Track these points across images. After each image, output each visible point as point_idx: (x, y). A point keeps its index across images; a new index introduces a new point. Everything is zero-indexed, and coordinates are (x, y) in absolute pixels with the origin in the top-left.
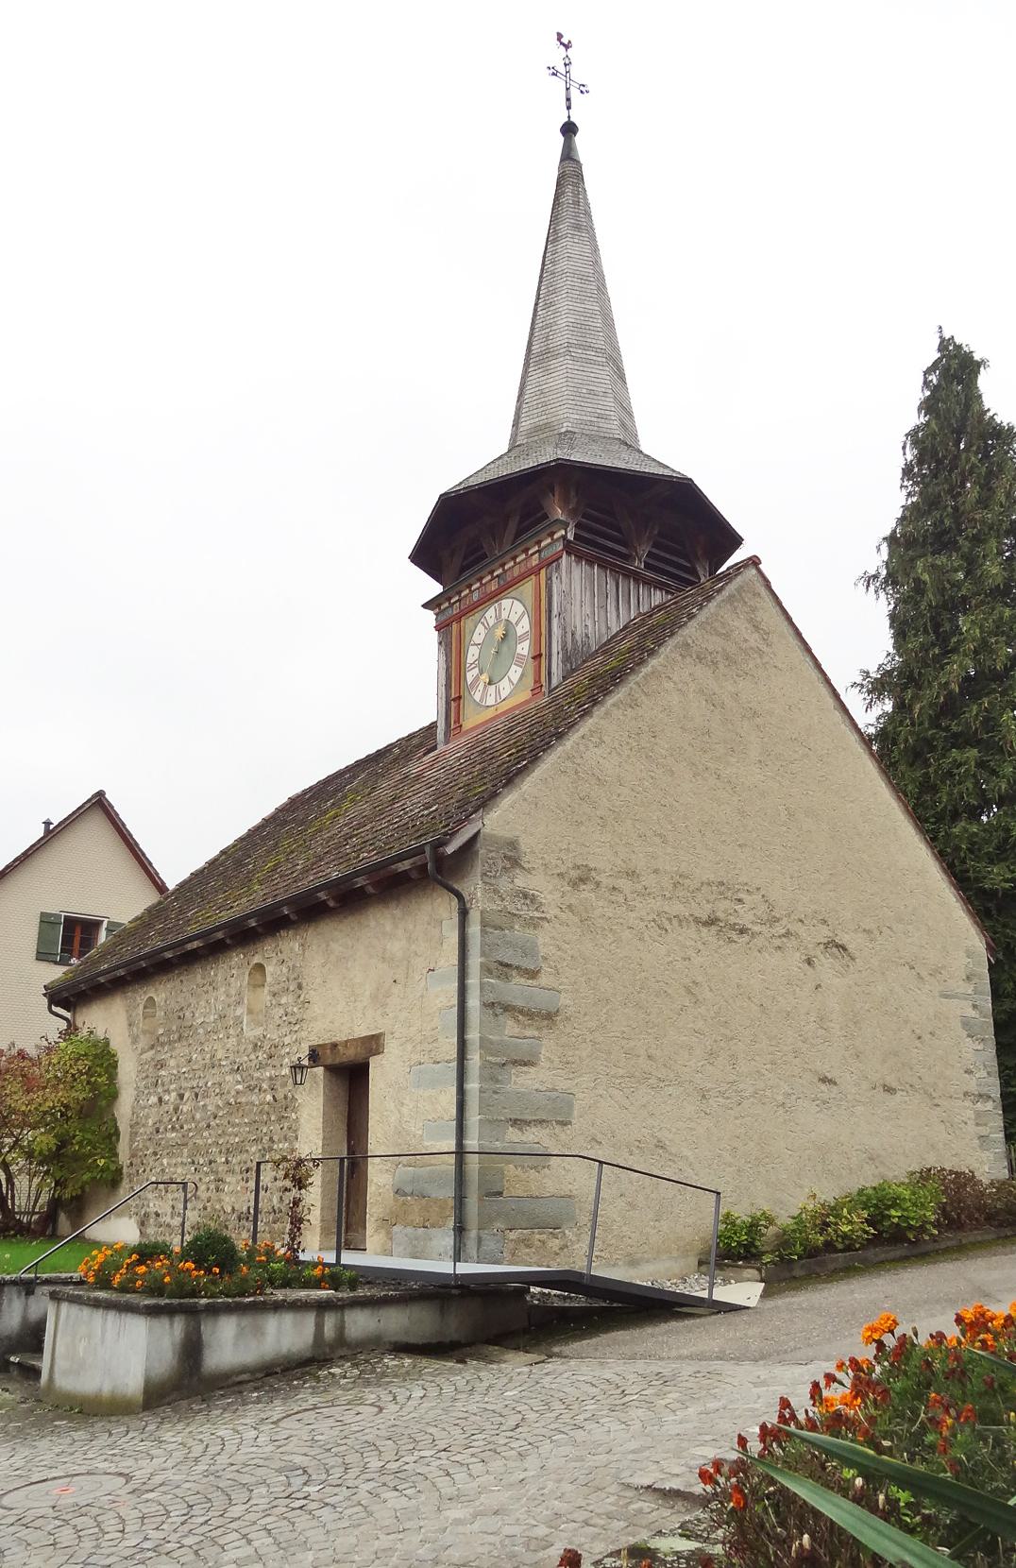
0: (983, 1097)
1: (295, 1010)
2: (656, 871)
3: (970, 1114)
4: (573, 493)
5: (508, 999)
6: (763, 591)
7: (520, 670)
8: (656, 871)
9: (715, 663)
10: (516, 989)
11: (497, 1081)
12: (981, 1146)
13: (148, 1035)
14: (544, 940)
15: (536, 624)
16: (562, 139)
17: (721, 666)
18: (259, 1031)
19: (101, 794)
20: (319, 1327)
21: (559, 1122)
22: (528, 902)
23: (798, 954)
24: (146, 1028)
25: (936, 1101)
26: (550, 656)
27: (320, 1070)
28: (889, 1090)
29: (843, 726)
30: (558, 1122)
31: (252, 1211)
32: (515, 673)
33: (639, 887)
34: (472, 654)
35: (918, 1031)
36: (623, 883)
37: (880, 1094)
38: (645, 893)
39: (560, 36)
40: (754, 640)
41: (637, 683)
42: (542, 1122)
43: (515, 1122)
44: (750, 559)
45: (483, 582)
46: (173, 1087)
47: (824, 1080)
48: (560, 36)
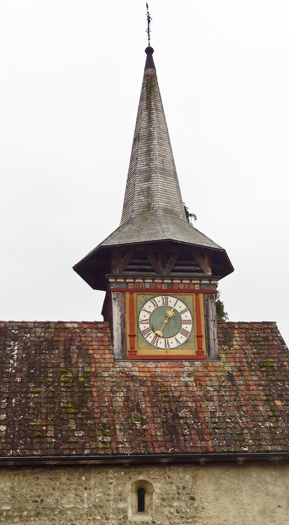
16: (146, 55)
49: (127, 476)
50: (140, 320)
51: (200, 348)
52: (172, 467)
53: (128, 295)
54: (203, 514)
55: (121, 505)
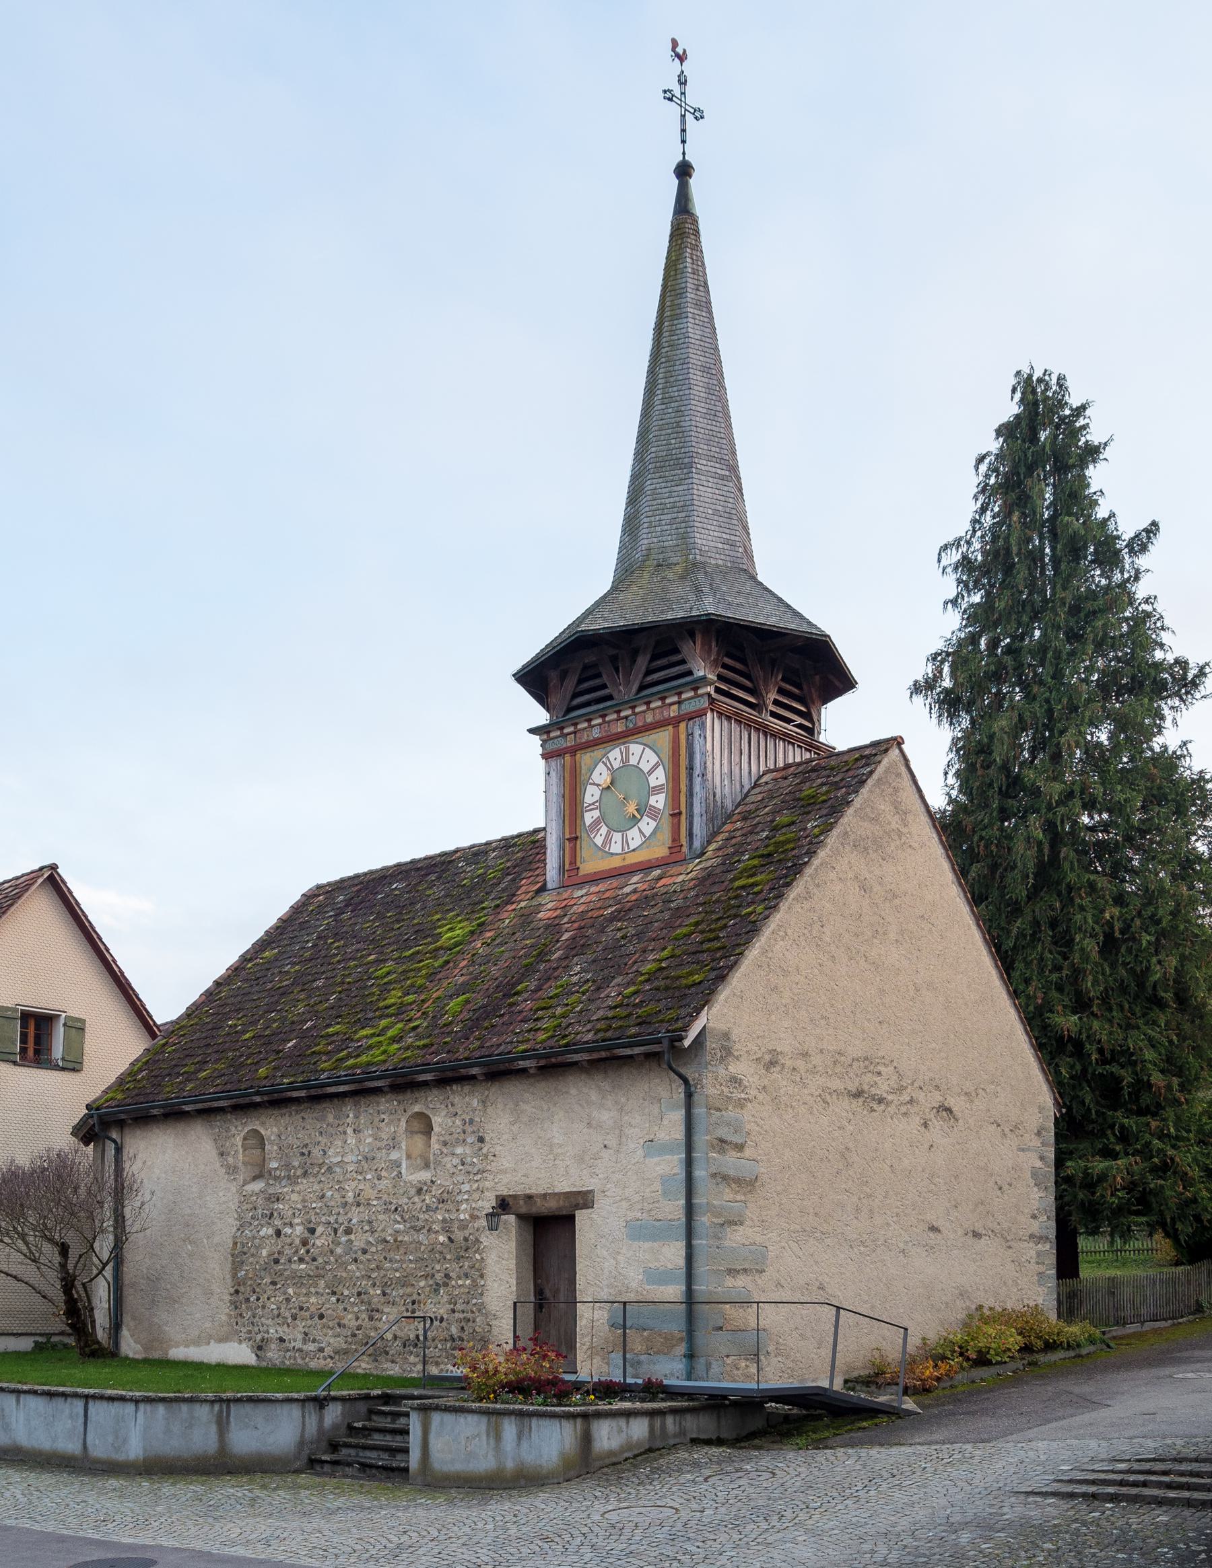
0: (1041, 1239)
1: (475, 1160)
3: (1033, 1253)
4: (714, 644)
5: (724, 1170)
6: (903, 770)
7: (653, 824)
8: (821, 1051)
9: (866, 849)
10: (730, 1162)
11: (719, 1239)
12: (1039, 1281)
13: (249, 1167)
14: (747, 1115)
15: (674, 778)
16: (677, 182)
18: (425, 1175)
19: (54, 867)
20: (652, 1428)
21: (757, 1271)
23: (918, 1118)
24: (247, 1159)
25: (1009, 1243)
27: (511, 1218)
28: (977, 1235)
30: (757, 1271)
31: (421, 1338)
34: (591, 795)
36: (801, 1064)
37: (970, 1240)
38: (813, 1071)
39: (675, 43)
40: (895, 821)
42: (745, 1270)
44: (894, 739)
46: (297, 1221)
47: (933, 1229)
48: (675, 43)
50: (585, 805)
51: (676, 838)
52: (454, 1087)
55: (394, 1155)
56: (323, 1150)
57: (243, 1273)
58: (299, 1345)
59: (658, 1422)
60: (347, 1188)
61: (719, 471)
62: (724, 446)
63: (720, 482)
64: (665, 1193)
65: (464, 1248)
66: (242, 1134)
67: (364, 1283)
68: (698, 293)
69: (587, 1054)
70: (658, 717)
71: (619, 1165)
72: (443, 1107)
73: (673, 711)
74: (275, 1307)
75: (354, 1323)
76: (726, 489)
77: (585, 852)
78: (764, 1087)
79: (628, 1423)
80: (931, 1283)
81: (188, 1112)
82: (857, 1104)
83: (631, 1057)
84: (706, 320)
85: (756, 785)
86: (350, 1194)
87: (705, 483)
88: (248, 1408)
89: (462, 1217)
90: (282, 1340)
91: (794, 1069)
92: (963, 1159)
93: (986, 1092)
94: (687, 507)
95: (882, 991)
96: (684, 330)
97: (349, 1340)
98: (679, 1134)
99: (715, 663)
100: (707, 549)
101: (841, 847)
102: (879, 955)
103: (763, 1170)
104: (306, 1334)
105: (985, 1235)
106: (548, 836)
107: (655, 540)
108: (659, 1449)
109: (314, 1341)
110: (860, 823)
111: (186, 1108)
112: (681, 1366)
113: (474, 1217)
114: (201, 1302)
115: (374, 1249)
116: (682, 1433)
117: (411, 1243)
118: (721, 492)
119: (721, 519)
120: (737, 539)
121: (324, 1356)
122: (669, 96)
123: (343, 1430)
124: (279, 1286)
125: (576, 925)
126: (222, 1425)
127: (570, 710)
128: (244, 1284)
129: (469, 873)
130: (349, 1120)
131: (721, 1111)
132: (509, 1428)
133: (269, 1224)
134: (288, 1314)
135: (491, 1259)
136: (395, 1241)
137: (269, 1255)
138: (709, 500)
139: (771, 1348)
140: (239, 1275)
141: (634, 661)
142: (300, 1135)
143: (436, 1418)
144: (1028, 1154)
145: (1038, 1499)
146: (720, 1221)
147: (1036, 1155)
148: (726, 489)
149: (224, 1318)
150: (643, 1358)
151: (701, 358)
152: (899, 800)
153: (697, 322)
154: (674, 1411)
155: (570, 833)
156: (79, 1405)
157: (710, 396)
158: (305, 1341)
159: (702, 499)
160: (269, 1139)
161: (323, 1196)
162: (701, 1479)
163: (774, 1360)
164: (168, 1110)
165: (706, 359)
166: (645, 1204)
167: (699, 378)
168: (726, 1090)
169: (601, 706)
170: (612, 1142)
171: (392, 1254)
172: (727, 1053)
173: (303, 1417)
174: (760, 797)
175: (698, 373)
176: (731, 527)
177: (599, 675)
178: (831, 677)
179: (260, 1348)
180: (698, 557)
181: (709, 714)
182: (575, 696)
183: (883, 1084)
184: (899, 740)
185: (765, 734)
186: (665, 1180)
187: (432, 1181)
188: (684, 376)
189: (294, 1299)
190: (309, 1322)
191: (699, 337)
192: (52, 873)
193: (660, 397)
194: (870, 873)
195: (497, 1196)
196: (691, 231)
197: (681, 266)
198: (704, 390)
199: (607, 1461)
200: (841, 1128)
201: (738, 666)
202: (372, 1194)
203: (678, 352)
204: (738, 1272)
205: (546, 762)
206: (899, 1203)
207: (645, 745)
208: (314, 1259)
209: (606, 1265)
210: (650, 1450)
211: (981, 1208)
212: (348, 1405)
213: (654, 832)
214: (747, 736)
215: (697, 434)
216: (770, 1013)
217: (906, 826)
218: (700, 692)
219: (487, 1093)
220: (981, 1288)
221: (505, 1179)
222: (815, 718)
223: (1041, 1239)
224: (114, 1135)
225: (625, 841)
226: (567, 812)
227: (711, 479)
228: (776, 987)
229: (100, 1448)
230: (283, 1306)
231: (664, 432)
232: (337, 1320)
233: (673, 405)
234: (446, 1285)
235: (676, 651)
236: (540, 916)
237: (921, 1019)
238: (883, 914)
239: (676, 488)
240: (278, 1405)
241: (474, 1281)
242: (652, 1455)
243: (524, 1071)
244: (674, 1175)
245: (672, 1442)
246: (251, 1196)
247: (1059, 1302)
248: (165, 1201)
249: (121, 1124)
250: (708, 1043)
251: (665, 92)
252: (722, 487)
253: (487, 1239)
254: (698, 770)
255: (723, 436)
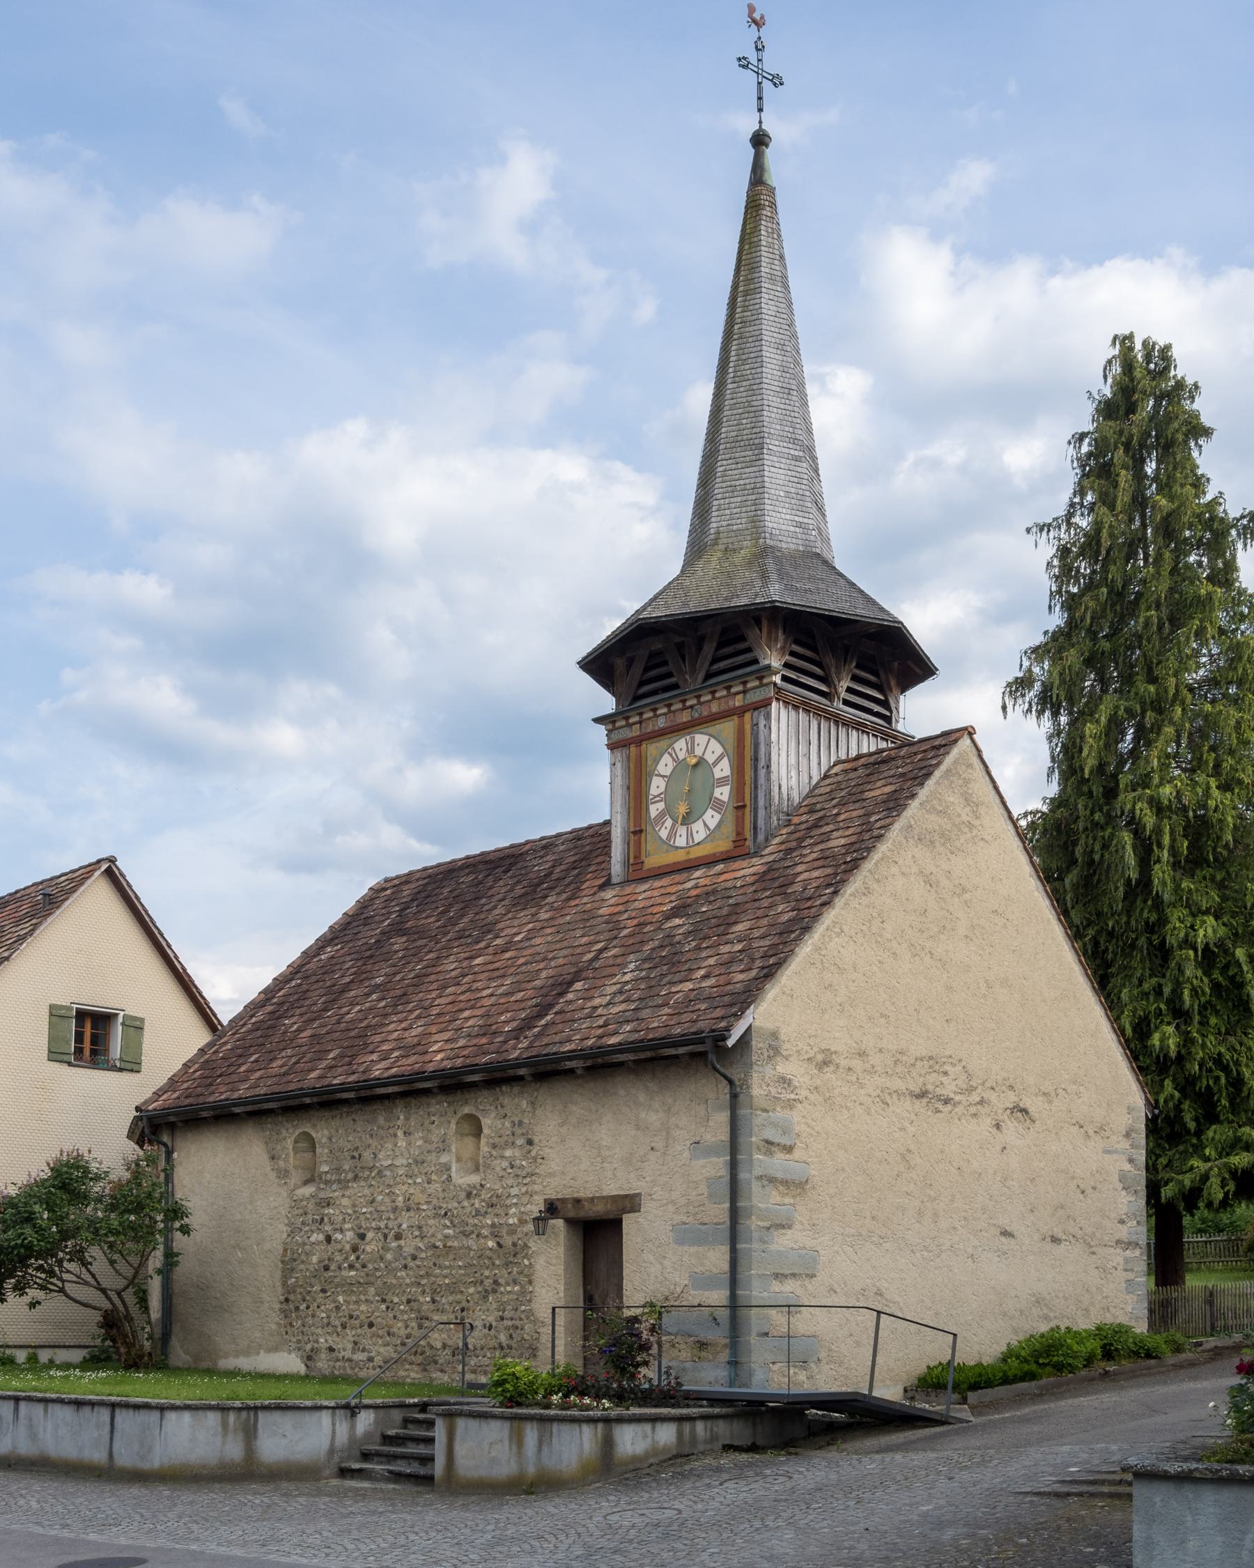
0: (1130, 1245)
1: (524, 1163)
2: (881, 1051)
3: (1121, 1260)
5: (771, 1172)
7: (718, 817)
8: (881, 1051)
9: (932, 842)
10: (777, 1163)
11: (765, 1242)
12: (1127, 1289)
14: (797, 1118)
15: (738, 769)
17: (937, 844)
18: (474, 1179)
19: (112, 860)
20: (680, 1435)
21: (807, 1275)
22: (786, 1085)
23: (989, 1120)
25: (1093, 1249)
26: (756, 809)
27: (559, 1223)
28: (1055, 1240)
29: (1036, 893)
30: (807, 1275)
32: (712, 818)
33: (868, 1066)
34: (657, 786)
35: (1082, 1186)
36: (857, 1064)
37: (1048, 1246)
38: (872, 1071)
39: (751, 9)
40: (965, 814)
41: (870, 871)
42: (794, 1275)
43: (777, 1276)
44: (965, 729)
45: (672, 709)
46: (347, 1226)
47: (1006, 1234)
48: (751, 9)
49: (452, 1109)
50: (651, 797)
52: (504, 1088)
53: (633, 748)
54: (541, 1170)
55: (444, 1159)
56: (374, 1154)
57: (293, 1280)
58: (348, 1354)
59: (687, 1427)
60: (397, 1192)
61: (792, 452)
62: (798, 426)
63: (793, 462)
64: (710, 1196)
65: (512, 1253)
66: (293, 1138)
67: (414, 1289)
68: (773, 267)
69: (633, 1054)
70: (724, 707)
71: (665, 1168)
72: (492, 1108)
73: (738, 701)
74: (324, 1315)
75: (403, 1332)
76: (799, 470)
77: (649, 845)
78: (816, 1088)
79: (653, 1429)
80: (1004, 1289)
81: (238, 1114)
82: (919, 1105)
83: (676, 1056)
84: (781, 295)
85: (826, 777)
86: (400, 1199)
87: (777, 465)
88: (277, 1416)
89: (511, 1221)
90: (331, 1349)
91: (850, 1069)
92: (1040, 1161)
93: (1067, 1093)
94: (758, 489)
95: (949, 988)
96: (757, 306)
97: (399, 1349)
98: (724, 1136)
99: (782, 651)
100: (778, 532)
101: (904, 841)
102: (947, 951)
103: (814, 1172)
104: (355, 1343)
105: (1066, 1240)
106: (613, 829)
107: (725, 523)
108: (688, 1456)
109: (363, 1350)
110: (926, 816)
111: (237, 1110)
112: (725, 1373)
113: (522, 1222)
114: (251, 1311)
115: (423, 1255)
116: (713, 1438)
117: (461, 1248)
118: (794, 474)
119: (793, 501)
120: (810, 521)
121: (373, 1366)
122: (743, 63)
123: (378, 1439)
124: (329, 1294)
125: (635, 922)
126: (250, 1434)
127: (636, 698)
128: (294, 1292)
129: (540, 867)
130: (399, 1123)
131: (767, 1111)
132: (531, 1434)
133: (320, 1229)
134: (337, 1323)
135: (540, 1264)
136: (445, 1246)
137: (320, 1262)
138: (781, 482)
139: (822, 1355)
140: (289, 1283)
141: (700, 649)
142: (350, 1138)
143: (461, 1423)
144: (1115, 1156)
145: (1035, 1499)
146: (766, 1224)
147: (1124, 1158)
148: (799, 470)
149: (274, 1327)
150: (688, 1365)
151: (775, 335)
152: (970, 791)
153: (771, 297)
154: (704, 1417)
155: (635, 826)
156: (105, 1414)
157: (784, 374)
158: (354, 1352)
159: (773, 480)
160: (320, 1142)
161: (373, 1201)
162: (717, 1483)
163: (825, 1368)
164: (218, 1112)
165: (780, 336)
166: (691, 1208)
167: (772, 356)
168: (773, 1091)
169: (667, 695)
170: (659, 1144)
171: (441, 1261)
172: (775, 1051)
173: (334, 1424)
174: (828, 789)
175: (772, 350)
176: (804, 509)
177: (665, 663)
178: (910, 663)
179: (309, 1358)
180: (768, 541)
181: (774, 704)
182: (642, 684)
183: (949, 1084)
184: (970, 729)
185: (837, 723)
186: (710, 1182)
187: (481, 1185)
188: (756, 354)
189: (344, 1307)
190: (359, 1331)
191: (773, 314)
192: (110, 866)
193: (732, 375)
194: (938, 867)
195: (545, 1200)
196: (767, 203)
197: (756, 239)
198: (777, 368)
199: (631, 1467)
200: (903, 1129)
201: (808, 653)
202: (421, 1198)
203: (751, 329)
204: (786, 1276)
205: (612, 753)
206: (968, 1207)
207: (710, 735)
208: (364, 1266)
209: (653, 1269)
210: (676, 1457)
211: (1060, 1212)
212: (382, 1412)
213: (719, 826)
214: (816, 726)
215: (769, 414)
216: (824, 1011)
217: (977, 818)
218: (765, 681)
219: (536, 1094)
220: (1061, 1295)
221: (554, 1182)
222: (893, 705)
223: (1130, 1245)
224: (165, 1139)
225: (690, 835)
226: (632, 805)
227: (783, 460)
228: (830, 986)
229: (126, 1457)
230: (333, 1315)
231: (735, 412)
232: (386, 1329)
233: (744, 383)
234: (495, 1291)
235: (743, 639)
236: (601, 912)
237: (994, 1017)
238: (951, 909)
239: (747, 470)
240: (306, 1413)
241: (522, 1287)
242: (679, 1460)
243: (571, 1071)
244: (720, 1177)
245: (701, 1448)
246: (301, 1200)
247: (1151, 1311)
248: (216, 1207)
249: (172, 1127)
250: (754, 1043)
251: (739, 59)
252: (796, 469)
253: (535, 1244)
254: (762, 763)
255: (797, 415)
